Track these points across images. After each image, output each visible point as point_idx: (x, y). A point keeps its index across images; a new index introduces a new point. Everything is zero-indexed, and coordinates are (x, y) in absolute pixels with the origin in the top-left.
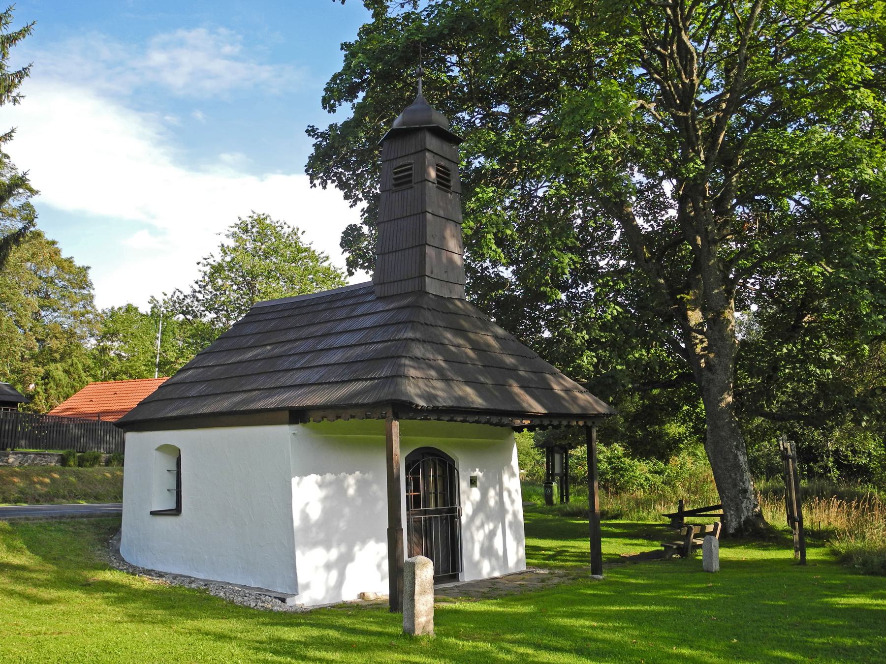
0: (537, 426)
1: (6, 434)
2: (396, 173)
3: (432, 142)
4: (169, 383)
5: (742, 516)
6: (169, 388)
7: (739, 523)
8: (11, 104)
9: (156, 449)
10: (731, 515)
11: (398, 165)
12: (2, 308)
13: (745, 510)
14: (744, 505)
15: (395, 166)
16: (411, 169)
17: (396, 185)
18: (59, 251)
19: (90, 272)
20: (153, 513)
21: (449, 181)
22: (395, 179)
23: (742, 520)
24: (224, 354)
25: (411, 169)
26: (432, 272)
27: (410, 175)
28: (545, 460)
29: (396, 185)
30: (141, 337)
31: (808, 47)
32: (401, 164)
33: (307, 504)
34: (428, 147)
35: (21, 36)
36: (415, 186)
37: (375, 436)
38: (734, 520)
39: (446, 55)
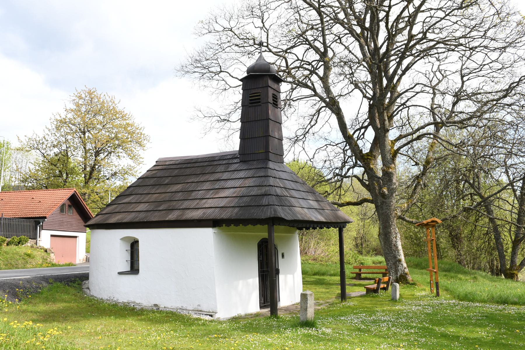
0: (304, 228)
7: (397, 277)
9: (122, 239)
10: (393, 273)
11: (252, 93)
14: (399, 268)
15: (250, 93)
18: (512, 279)
19: (348, 226)
20: (120, 273)
22: (251, 100)
23: (398, 275)
25: (260, 95)
27: (259, 99)
29: (251, 103)
30: (104, 178)
32: (254, 92)
33: (120, 273)
34: (269, 85)
39: (379, 178)
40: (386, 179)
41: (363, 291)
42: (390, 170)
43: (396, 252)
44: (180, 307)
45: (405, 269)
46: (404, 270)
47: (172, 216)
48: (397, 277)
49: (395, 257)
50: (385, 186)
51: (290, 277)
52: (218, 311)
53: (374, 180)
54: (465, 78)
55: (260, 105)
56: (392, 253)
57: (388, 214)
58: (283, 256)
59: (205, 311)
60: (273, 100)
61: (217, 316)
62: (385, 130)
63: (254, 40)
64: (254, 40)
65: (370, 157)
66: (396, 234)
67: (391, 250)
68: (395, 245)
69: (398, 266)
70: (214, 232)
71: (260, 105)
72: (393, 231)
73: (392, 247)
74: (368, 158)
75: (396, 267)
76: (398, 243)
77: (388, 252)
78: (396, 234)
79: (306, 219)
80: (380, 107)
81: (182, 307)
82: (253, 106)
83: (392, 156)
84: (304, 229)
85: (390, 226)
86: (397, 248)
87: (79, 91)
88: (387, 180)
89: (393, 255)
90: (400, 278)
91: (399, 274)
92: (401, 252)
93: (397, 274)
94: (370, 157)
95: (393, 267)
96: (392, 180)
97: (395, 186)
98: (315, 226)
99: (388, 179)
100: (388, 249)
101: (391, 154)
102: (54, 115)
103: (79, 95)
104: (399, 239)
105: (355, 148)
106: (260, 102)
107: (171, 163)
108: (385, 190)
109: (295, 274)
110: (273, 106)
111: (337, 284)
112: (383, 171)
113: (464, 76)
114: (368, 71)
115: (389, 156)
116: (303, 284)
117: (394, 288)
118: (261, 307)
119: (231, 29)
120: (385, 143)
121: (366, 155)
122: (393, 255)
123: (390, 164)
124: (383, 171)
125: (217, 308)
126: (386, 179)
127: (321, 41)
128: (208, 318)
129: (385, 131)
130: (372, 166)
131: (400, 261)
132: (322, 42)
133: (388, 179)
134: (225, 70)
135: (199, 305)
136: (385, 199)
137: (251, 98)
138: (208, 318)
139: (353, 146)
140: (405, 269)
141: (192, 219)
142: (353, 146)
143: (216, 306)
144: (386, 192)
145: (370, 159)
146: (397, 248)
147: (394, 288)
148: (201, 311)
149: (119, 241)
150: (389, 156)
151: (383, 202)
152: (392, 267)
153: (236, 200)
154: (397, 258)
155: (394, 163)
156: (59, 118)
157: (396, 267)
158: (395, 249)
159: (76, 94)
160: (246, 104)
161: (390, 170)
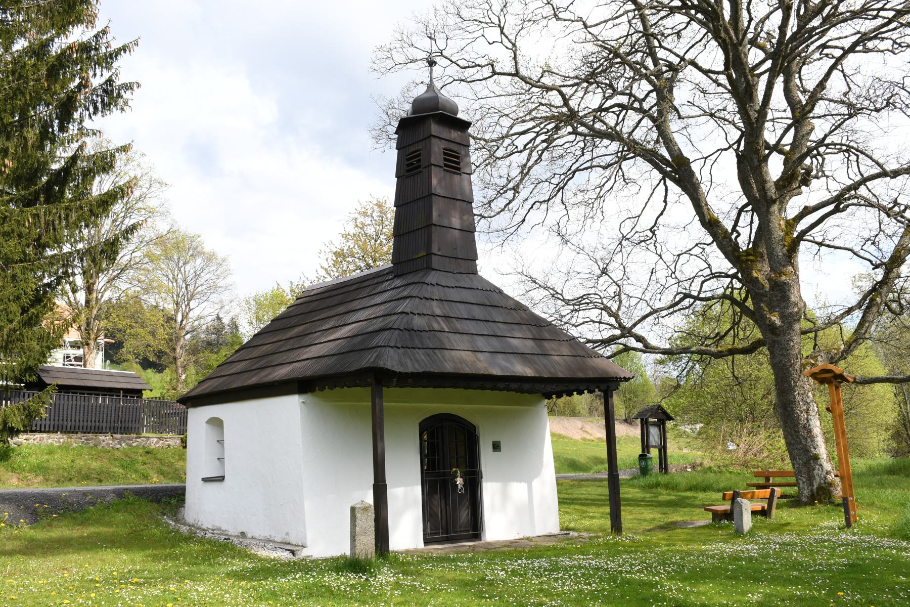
1: (82, 409)
2: (408, 160)
3: (435, 129)
4: (228, 361)
5: (814, 483)
6: (225, 366)
7: (812, 490)
8: (119, 111)
10: (803, 483)
12: (2, 311)
13: (817, 477)
14: (816, 472)
16: (419, 155)
17: (408, 171)
20: (206, 480)
21: (458, 163)
24: (272, 333)
25: (419, 155)
26: (439, 250)
28: (835, 449)
29: (446, 165)
31: (46, 232)
32: (412, 150)
33: (206, 480)
35: (122, 52)
36: (424, 170)
37: (393, 404)
38: (806, 488)
40: (776, 296)
41: (705, 519)
42: (783, 278)
43: (809, 440)
45: (827, 473)
46: (825, 478)
48: (812, 490)
49: (807, 451)
51: (518, 490)
52: (309, 543)
53: (762, 301)
55: (421, 172)
56: (801, 443)
57: (784, 365)
58: (496, 447)
59: (294, 543)
60: (445, 160)
61: (304, 553)
62: (767, 201)
63: (492, 66)
64: (492, 66)
65: (751, 258)
66: (808, 404)
67: (797, 437)
68: (804, 427)
69: (814, 469)
70: (303, 402)
72: (799, 398)
73: (798, 432)
74: (748, 260)
75: (809, 472)
76: (811, 423)
77: (792, 442)
78: (808, 404)
79: (467, 370)
80: (752, 158)
83: (788, 251)
84: (554, 396)
85: (792, 389)
86: (811, 432)
87: (364, 204)
88: (779, 298)
89: (801, 446)
90: (817, 492)
91: (815, 486)
92: (820, 440)
93: (811, 484)
94: (751, 258)
95: (804, 470)
96: (788, 298)
97: (796, 309)
98: (581, 388)
99: (780, 295)
101: (784, 246)
102: (327, 244)
103: (363, 210)
104: (813, 414)
105: (724, 243)
107: (319, 291)
109: (536, 483)
110: (445, 170)
111: (626, 500)
112: (770, 280)
114: (729, 92)
115: (780, 251)
116: (559, 503)
118: (427, 542)
119: (441, 53)
120: (769, 226)
121: (744, 254)
122: (801, 446)
123: (784, 266)
124: (768, 280)
125: (305, 538)
126: (776, 296)
129: (767, 203)
130: (755, 275)
131: (816, 458)
133: (780, 295)
134: (858, 173)
136: (778, 335)
139: (720, 239)
140: (827, 473)
142: (720, 239)
143: (305, 534)
144: (778, 322)
145: (752, 261)
146: (810, 431)
149: (205, 425)
150: (780, 251)
151: (774, 341)
152: (800, 472)
154: (811, 452)
155: (792, 265)
156: (335, 250)
157: (809, 472)
158: (805, 434)
159: (359, 209)
160: (402, 174)
161: (783, 278)
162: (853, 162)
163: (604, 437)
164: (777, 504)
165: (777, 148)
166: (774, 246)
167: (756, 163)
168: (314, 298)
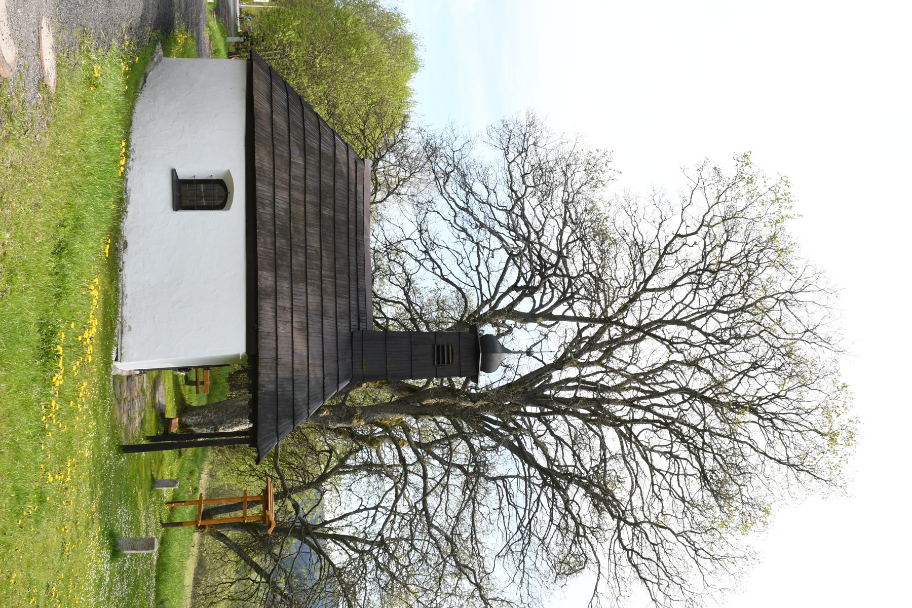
7: (191, 426)
9: (229, 171)
29: (438, 347)
32: (455, 352)
44: (125, 293)
47: (266, 278)
48: (191, 426)
50: (330, 412)
54: (500, 482)
55: (434, 364)
56: (227, 419)
67: (232, 417)
68: (240, 422)
71: (434, 364)
73: (236, 418)
75: (205, 424)
81: (126, 297)
82: (434, 351)
93: (195, 425)
95: (207, 420)
100: (234, 412)
106: (438, 363)
107: (360, 195)
108: (325, 413)
113: (504, 481)
117: (171, 483)
123: (365, 420)
125: (128, 361)
126: (342, 414)
127: (567, 314)
128: (114, 357)
132: (565, 314)
135: (130, 329)
137: (445, 347)
138: (114, 357)
141: (259, 320)
147: (171, 483)
148: (122, 333)
149: (226, 169)
152: (205, 418)
153: (288, 375)
157: (205, 424)
162: (583, 373)
163: (258, 184)
164: (153, 549)
165: (245, 513)
166: (382, 414)
167: (446, 413)
168: (352, 188)
